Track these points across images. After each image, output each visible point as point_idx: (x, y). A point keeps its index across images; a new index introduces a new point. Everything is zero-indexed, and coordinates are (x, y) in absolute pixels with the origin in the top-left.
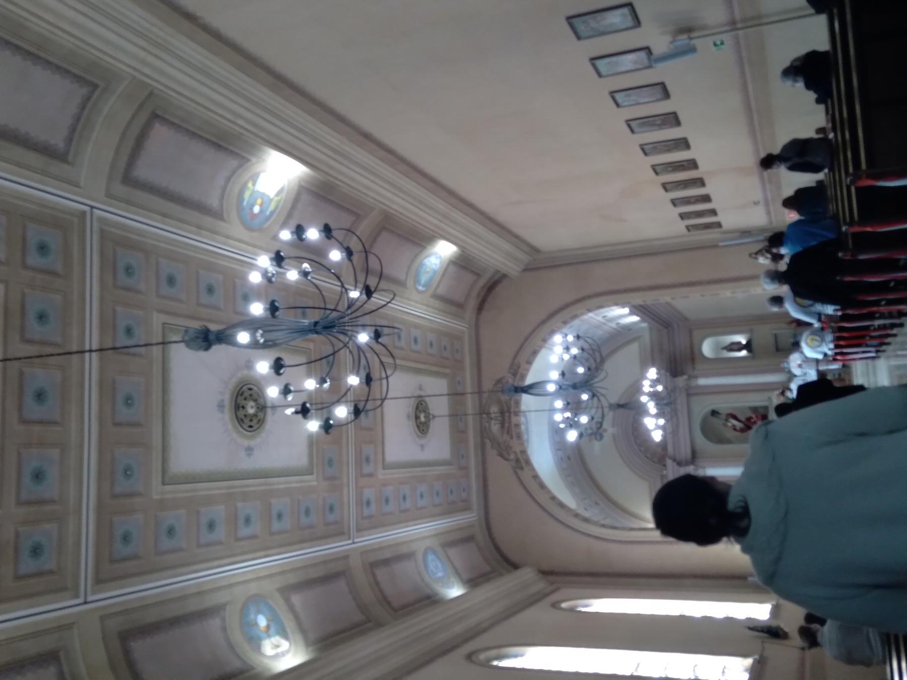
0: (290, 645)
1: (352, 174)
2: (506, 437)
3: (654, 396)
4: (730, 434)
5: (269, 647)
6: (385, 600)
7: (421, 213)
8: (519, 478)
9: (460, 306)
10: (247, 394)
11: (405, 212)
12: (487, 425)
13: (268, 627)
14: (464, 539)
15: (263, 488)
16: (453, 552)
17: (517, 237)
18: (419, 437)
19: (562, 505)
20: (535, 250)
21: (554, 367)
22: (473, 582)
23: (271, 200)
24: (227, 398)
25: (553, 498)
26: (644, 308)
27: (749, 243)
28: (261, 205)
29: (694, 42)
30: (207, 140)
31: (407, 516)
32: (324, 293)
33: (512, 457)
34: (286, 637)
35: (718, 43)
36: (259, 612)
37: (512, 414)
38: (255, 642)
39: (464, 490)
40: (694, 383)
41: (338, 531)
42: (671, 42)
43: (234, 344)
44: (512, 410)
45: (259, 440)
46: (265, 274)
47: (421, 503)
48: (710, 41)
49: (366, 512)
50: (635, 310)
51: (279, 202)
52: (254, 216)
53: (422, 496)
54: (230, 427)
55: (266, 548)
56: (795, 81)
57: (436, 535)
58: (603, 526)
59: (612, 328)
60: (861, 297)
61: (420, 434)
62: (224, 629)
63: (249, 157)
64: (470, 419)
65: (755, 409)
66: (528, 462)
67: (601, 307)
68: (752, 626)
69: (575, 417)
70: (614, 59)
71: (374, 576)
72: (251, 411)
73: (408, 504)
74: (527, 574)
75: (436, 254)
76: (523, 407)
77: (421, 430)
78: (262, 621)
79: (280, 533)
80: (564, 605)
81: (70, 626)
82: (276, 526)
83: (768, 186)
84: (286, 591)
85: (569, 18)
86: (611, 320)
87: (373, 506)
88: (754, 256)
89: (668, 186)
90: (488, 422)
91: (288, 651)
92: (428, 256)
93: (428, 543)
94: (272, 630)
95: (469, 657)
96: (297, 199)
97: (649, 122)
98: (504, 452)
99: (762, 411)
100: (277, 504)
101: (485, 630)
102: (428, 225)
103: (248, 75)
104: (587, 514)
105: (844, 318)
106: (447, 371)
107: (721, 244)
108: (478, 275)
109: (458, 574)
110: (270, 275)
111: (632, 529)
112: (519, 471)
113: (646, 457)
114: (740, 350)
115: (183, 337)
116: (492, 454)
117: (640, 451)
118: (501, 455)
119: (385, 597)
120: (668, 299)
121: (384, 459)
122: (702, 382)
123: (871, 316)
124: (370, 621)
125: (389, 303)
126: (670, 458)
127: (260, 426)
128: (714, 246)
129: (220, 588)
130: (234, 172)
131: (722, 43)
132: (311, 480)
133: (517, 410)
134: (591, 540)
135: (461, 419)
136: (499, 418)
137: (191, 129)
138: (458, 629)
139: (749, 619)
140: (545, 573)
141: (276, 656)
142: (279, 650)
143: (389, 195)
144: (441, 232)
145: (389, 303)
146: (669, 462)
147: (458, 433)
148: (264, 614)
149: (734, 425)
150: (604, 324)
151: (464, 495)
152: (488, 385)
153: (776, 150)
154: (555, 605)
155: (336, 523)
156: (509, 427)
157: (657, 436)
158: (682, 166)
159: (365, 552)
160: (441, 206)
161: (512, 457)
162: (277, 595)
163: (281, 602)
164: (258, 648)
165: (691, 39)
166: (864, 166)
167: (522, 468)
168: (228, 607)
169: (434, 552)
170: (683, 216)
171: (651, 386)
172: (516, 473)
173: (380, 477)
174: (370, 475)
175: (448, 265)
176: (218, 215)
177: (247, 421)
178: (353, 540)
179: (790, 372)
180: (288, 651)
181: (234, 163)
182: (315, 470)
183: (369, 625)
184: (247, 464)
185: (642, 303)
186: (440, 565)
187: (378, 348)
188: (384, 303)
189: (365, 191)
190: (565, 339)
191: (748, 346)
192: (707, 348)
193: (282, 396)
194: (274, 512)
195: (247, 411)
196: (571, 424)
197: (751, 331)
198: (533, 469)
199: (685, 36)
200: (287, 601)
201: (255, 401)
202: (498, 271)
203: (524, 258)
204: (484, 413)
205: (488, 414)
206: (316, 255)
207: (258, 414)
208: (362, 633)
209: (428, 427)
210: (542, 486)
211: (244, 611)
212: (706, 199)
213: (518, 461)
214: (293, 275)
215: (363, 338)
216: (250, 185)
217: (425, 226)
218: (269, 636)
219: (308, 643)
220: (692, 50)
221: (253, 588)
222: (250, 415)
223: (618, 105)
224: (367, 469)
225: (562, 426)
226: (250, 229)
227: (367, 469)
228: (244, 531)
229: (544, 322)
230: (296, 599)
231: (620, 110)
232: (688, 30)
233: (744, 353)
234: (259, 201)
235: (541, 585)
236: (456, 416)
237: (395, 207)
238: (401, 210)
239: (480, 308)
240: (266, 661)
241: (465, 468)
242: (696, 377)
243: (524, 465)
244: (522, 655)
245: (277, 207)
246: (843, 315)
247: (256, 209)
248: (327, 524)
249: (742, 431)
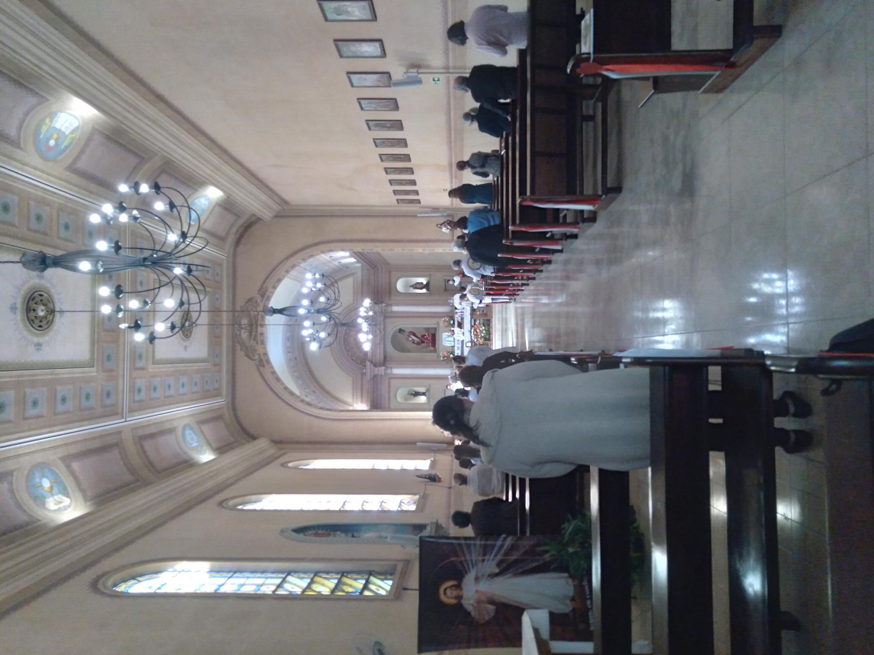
0: (71, 501)
2: (252, 342)
3: (366, 318)
4: (410, 345)
5: (51, 504)
6: (150, 465)
8: (261, 374)
9: (222, 239)
10: (38, 299)
11: (185, 161)
12: (238, 333)
13: (51, 488)
14: (214, 418)
15: (50, 377)
16: (206, 428)
17: (271, 190)
18: (184, 340)
19: (292, 394)
20: (285, 202)
21: (306, 296)
22: (221, 450)
23: (66, 137)
24: (19, 302)
25: (286, 388)
26: (361, 254)
27: (438, 216)
28: (56, 140)
29: (420, 76)
30: (9, 77)
31: (170, 401)
32: (154, 236)
33: (256, 357)
34: (67, 495)
35: (436, 79)
36: (43, 476)
37: (259, 326)
38: (40, 500)
39: (217, 382)
40: (389, 309)
41: (112, 412)
42: (405, 73)
43: (75, 270)
44: (259, 323)
45: (47, 338)
46: (104, 216)
47: (181, 391)
48: (431, 77)
49: (137, 398)
50: (355, 254)
51: (73, 139)
52: (49, 148)
53: (183, 385)
54: (21, 326)
55: (50, 426)
56: (467, 91)
57: (193, 415)
58: (321, 408)
59: (335, 265)
60: (510, 267)
61: (185, 338)
62: (12, 491)
63: (47, 97)
64: (225, 328)
65: (427, 329)
66: (268, 361)
67: (331, 251)
68: (419, 474)
69: (317, 333)
70: (364, 76)
71: (142, 447)
72: (41, 314)
73: (172, 392)
74: (262, 443)
75: (205, 196)
76: (267, 322)
77: (185, 335)
78: (46, 484)
79: (64, 413)
80: (290, 465)
82: (60, 408)
83: (454, 180)
84: (67, 460)
85: (335, 41)
86: (335, 260)
87: (143, 394)
88: (439, 226)
89: (388, 170)
90: (239, 331)
91: (69, 506)
92: (198, 198)
93: (187, 421)
94: (55, 490)
95: (221, 504)
96: (90, 139)
97: (382, 124)
98: (250, 353)
99: (432, 332)
100: (61, 390)
101: (232, 484)
102: (201, 173)
103: (56, 29)
104: (307, 399)
105: (496, 278)
107: (418, 215)
108: (238, 216)
109: (209, 444)
110: (109, 218)
111: (336, 410)
112: (261, 368)
113: (352, 359)
114: (421, 288)
115: (21, 259)
116: (240, 354)
117: (348, 355)
118: (248, 356)
119: (151, 463)
120: (379, 250)
121: (153, 357)
122: (395, 309)
123: (512, 278)
125: (204, 248)
126: (369, 361)
127: (48, 327)
128: (414, 216)
129: (8, 458)
130: (32, 109)
131: (438, 80)
132: (92, 372)
133: (262, 323)
134: (313, 419)
135: (217, 328)
136: (248, 328)
138: (210, 484)
139: (416, 470)
140: (275, 442)
141: (59, 510)
142: (61, 505)
143: (173, 146)
144: (212, 180)
145: (204, 248)
146: (368, 363)
147: (214, 339)
148: (47, 478)
149: (413, 340)
150: (330, 262)
151: (216, 385)
152: (240, 303)
153: (466, 158)
154: (284, 465)
155: (113, 405)
156: (256, 336)
157: (367, 347)
158: (401, 158)
159: (135, 428)
160: (215, 160)
161: (256, 357)
162: (60, 463)
163: (63, 469)
164: (43, 505)
165: (419, 73)
166: (528, 193)
167: (264, 366)
168: (15, 474)
169: (192, 429)
170: (395, 192)
171: (366, 312)
172: (259, 370)
173: (150, 370)
174: (143, 369)
175: (215, 206)
176: (16, 144)
177: (37, 321)
178: (126, 419)
179: (453, 306)
180: (69, 506)
181: (33, 100)
182: (95, 363)
183: (138, 483)
184: (36, 357)
185: (360, 251)
186: (195, 437)
187: (191, 278)
188: (201, 248)
189: (153, 141)
190: (314, 276)
191: (427, 286)
192: (400, 285)
193: (115, 313)
194: (59, 397)
195: (37, 314)
196: (314, 338)
197: (430, 276)
198: (272, 367)
199: (415, 71)
200: (69, 467)
201: (45, 305)
202: (254, 215)
203: (276, 208)
204: (237, 325)
205: (240, 325)
206: (144, 206)
207: (48, 316)
208: (133, 490)
209: (191, 332)
210: (278, 379)
211: (29, 477)
212: (413, 183)
213: (261, 360)
214: (124, 218)
215: (178, 271)
216: (47, 121)
217: (200, 175)
218: (52, 495)
219: (86, 499)
220: (419, 82)
221: (39, 458)
222: (40, 317)
223: (362, 109)
224: (140, 364)
225: (308, 339)
226: (45, 159)
227: (140, 364)
228: (32, 412)
229: (287, 258)
230: (76, 465)
231: (363, 112)
232: (418, 66)
233: (424, 291)
234: (55, 136)
235: (272, 451)
236: (214, 325)
238: (180, 158)
239: (238, 242)
240: (50, 514)
241: (218, 365)
242: (391, 305)
243: (265, 364)
244: (260, 501)
245: (71, 143)
246: (496, 276)
247: (52, 143)
248: (104, 406)
249: (418, 344)
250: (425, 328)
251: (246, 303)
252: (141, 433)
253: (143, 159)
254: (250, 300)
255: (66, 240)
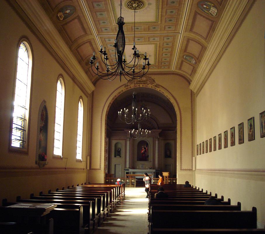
1: (221, 30)
6: (79, 46)
7: (206, 61)
11: (206, 55)
49: (107, 40)
71: (87, 42)
72: (134, 5)
81: (91, 34)
106: (157, 64)
119: (80, 46)
124: (72, 43)
134: (102, 108)
137: (202, 52)
140: (93, 92)
155: (102, 31)
167: (125, 87)
203: (195, 91)
212: (226, 146)
237: (207, 52)
250: (148, 156)
251: (152, 79)
252: (92, 41)
253: (206, 39)
254: (154, 81)
255: (166, 12)
